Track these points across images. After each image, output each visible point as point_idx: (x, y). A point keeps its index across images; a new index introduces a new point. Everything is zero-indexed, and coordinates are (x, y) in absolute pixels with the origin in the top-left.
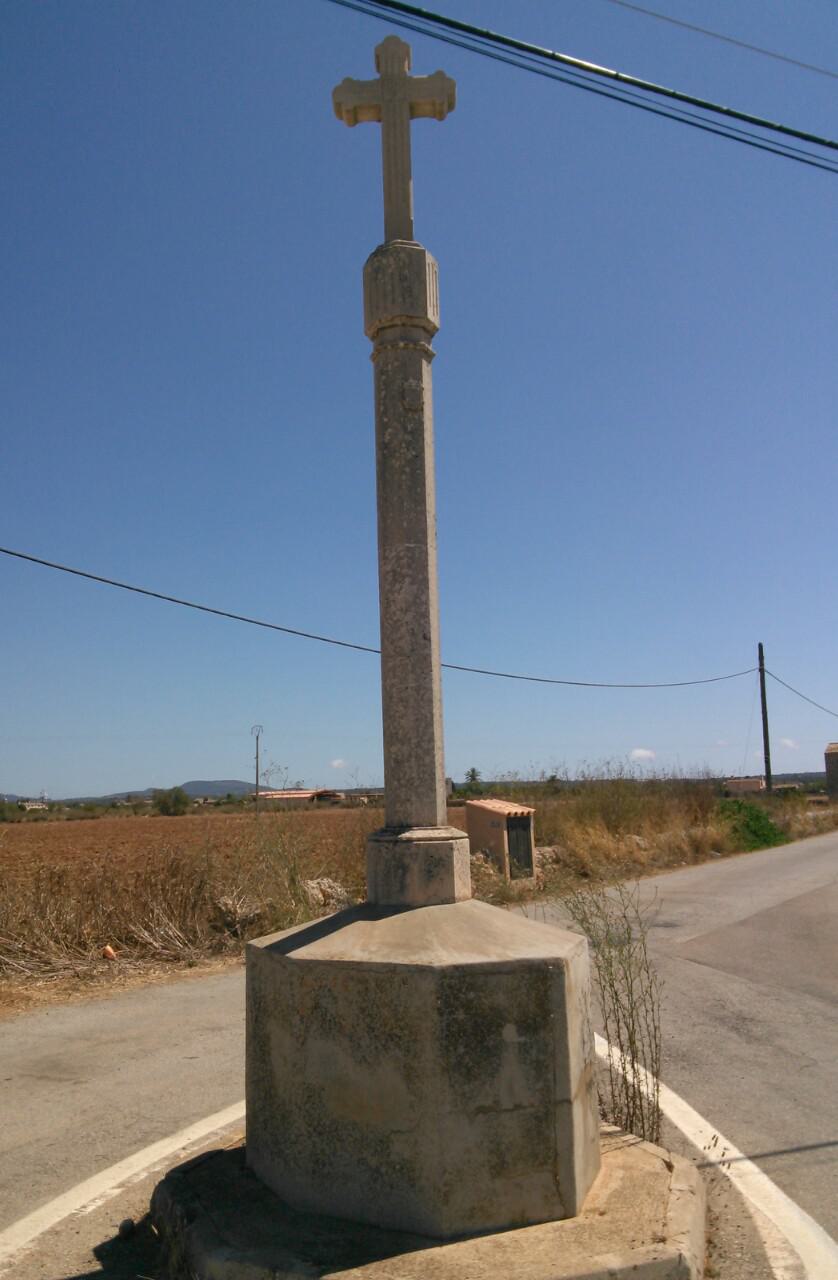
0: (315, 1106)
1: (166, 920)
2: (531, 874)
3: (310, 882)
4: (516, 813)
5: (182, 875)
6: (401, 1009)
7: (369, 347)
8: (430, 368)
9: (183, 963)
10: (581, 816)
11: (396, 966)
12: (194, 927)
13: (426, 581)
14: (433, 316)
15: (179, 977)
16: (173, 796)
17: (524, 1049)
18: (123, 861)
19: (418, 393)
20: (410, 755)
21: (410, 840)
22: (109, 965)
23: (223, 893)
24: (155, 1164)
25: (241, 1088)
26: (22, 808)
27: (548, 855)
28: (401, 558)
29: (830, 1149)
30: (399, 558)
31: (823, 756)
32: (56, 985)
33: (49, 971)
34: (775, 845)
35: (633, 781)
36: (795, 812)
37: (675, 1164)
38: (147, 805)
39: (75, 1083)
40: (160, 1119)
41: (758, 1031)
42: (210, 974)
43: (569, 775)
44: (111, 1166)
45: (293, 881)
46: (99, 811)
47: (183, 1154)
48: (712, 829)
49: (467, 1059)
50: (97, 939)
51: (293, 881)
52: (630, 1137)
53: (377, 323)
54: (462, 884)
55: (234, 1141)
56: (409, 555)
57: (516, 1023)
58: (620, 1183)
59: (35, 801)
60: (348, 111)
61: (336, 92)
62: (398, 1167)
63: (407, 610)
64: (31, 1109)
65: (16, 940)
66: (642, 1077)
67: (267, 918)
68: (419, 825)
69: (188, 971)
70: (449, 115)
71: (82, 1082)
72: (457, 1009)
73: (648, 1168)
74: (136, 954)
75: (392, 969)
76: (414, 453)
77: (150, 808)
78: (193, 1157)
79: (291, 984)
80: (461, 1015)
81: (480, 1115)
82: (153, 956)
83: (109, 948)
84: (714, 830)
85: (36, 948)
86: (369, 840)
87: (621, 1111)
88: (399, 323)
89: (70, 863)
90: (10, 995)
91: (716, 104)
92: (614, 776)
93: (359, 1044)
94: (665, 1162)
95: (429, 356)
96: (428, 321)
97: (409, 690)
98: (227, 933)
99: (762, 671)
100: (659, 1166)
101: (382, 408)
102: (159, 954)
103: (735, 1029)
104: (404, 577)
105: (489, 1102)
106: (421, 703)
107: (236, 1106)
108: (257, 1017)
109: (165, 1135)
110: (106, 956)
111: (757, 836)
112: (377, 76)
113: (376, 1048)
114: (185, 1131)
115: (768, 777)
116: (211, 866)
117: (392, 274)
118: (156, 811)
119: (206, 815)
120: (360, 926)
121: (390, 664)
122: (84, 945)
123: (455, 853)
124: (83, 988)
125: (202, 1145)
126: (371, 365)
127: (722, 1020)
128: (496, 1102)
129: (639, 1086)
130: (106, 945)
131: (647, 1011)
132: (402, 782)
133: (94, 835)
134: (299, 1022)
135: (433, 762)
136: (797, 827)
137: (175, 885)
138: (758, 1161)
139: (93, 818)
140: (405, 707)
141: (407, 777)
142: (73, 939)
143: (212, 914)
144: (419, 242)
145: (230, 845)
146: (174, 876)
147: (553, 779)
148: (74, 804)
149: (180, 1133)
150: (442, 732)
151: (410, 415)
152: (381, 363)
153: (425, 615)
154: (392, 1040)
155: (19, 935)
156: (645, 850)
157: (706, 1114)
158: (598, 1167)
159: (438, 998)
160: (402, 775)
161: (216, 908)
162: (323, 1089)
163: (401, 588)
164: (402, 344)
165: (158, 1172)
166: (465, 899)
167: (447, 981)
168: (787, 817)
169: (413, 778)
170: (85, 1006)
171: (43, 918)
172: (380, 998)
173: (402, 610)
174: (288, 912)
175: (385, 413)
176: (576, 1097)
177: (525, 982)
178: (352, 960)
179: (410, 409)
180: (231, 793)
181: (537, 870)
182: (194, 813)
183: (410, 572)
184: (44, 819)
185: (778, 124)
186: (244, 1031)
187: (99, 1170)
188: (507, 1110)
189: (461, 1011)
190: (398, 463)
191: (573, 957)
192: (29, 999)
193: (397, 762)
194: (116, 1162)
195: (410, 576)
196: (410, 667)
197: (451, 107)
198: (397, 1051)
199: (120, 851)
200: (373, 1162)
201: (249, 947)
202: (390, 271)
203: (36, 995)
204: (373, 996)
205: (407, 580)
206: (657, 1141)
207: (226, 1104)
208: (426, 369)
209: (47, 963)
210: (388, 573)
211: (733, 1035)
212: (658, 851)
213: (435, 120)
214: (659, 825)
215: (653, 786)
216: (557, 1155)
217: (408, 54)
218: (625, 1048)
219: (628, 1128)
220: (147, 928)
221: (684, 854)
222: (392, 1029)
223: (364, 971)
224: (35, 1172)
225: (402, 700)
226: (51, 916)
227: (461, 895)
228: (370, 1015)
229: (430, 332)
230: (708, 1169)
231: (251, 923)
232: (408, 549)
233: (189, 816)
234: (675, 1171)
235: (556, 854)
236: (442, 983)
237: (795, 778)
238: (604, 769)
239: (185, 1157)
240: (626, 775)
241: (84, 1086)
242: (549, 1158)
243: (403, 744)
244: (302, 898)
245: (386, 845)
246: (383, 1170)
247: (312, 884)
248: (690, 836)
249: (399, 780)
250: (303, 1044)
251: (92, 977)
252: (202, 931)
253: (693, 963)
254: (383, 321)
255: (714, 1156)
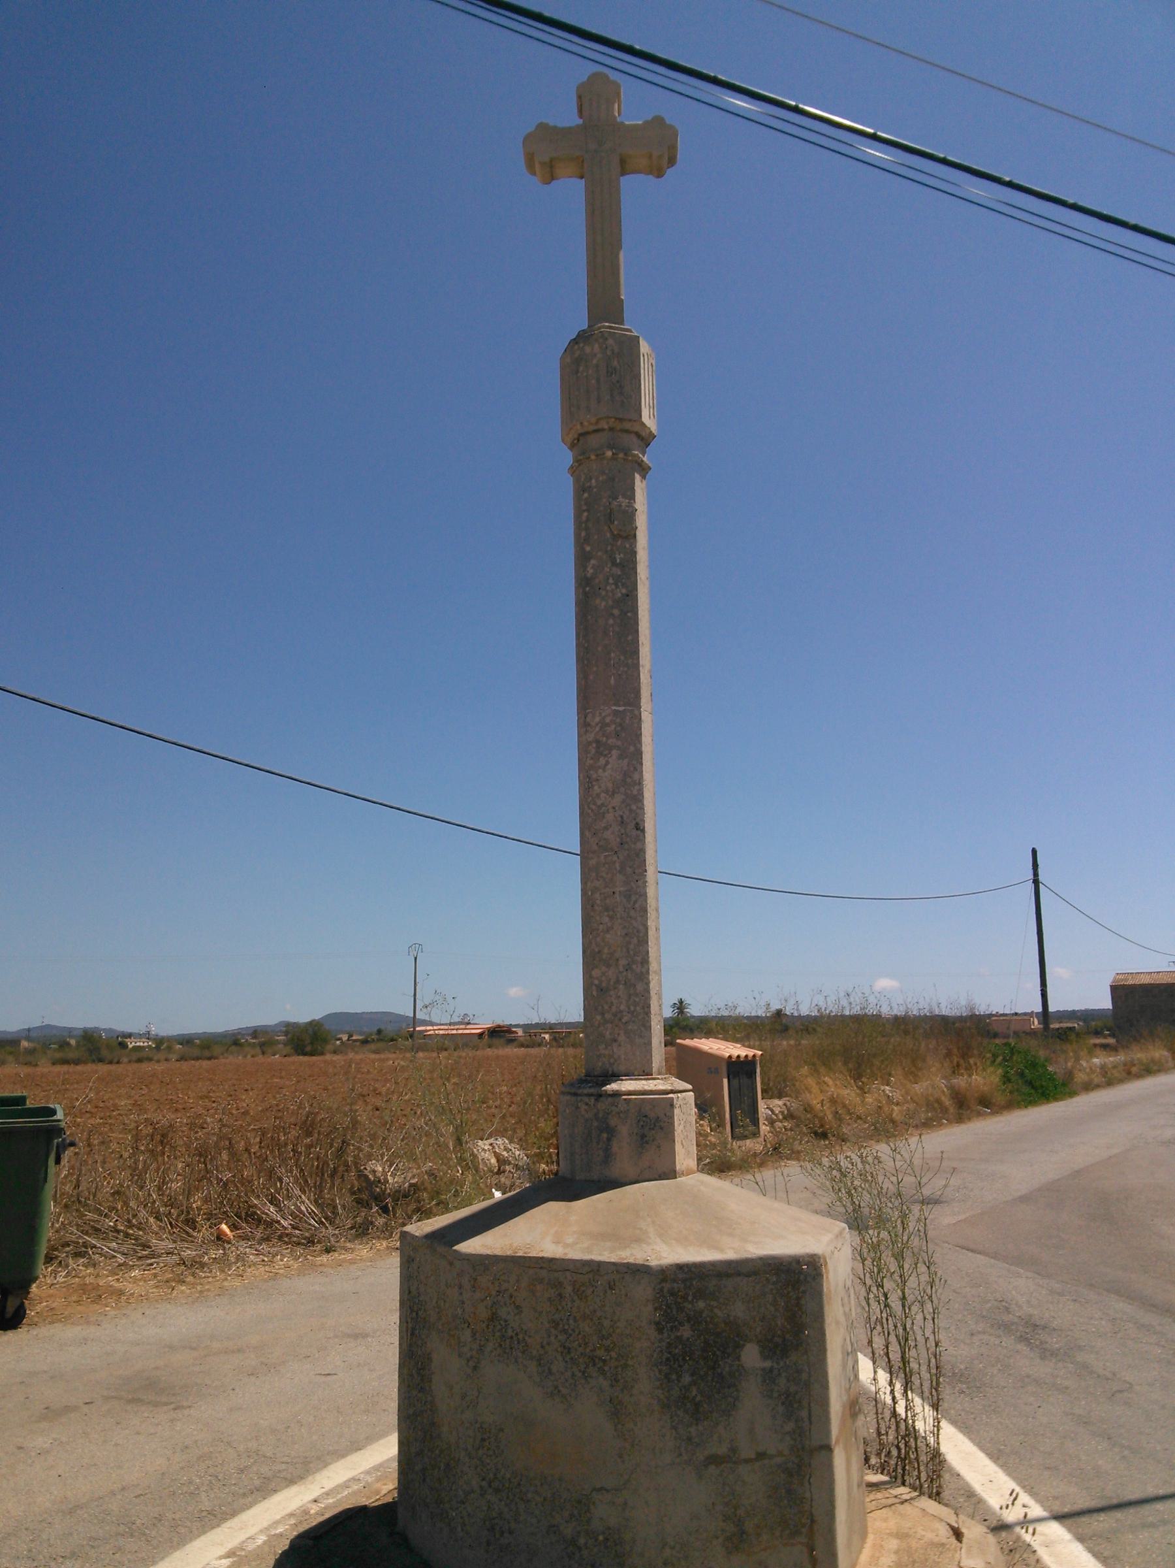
0: (491, 1452)
1: (297, 1192)
2: (756, 1134)
3: (480, 1143)
4: (738, 1057)
5: (319, 1133)
6: (606, 1323)
7: (567, 457)
8: (644, 482)
9: (318, 1247)
10: (822, 1060)
11: (600, 1264)
12: (333, 1200)
13: (639, 754)
14: (648, 418)
15: (313, 1265)
16: (310, 1032)
17: (769, 1376)
18: (246, 1113)
19: (629, 516)
20: (618, 982)
21: (617, 1094)
22: (224, 1249)
23: (369, 1157)
24: (277, 1523)
25: (392, 1417)
26: (123, 1045)
27: (777, 1111)
28: (608, 725)
29: (1159, 1506)
30: (604, 725)
31: (1109, 987)
32: (155, 1275)
33: (147, 1257)
34: (1056, 1099)
35: (879, 1016)
36: (1077, 1059)
37: (964, 1530)
38: (278, 1042)
39: (175, 1409)
40: (285, 1459)
41: (1054, 1342)
42: (352, 1262)
43: (801, 1007)
44: (218, 1526)
45: (459, 1141)
46: (217, 1050)
47: (314, 1509)
48: (979, 1079)
49: (694, 1392)
50: (209, 1216)
51: (459, 1141)
52: (903, 1491)
53: (579, 427)
54: (685, 1154)
55: (384, 1492)
56: (618, 720)
57: (759, 1342)
58: (893, 1557)
59: (140, 1036)
60: (542, 164)
61: (528, 139)
62: (601, 1538)
63: (613, 793)
64: (116, 1445)
65: (106, 1216)
66: (918, 1409)
67: (425, 1189)
68: (629, 1075)
69: (324, 1258)
70: (670, 172)
71: (183, 1407)
72: (681, 1324)
73: (929, 1536)
74: (259, 1236)
75: (595, 1268)
76: (624, 591)
77: (281, 1046)
78: (327, 1515)
79: (460, 1287)
80: (686, 1332)
81: (712, 1468)
82: (280, 1238)
83: (224, 1227)
84: (984, 1079)
85: (131, 1226)
86: (563, 1093)
87: (889, 1454)
88: (606, 427)
89: (179, 1115)
90: (97, 1287)
91: (997, 175)
92: (856, 1010)
93: (549, 1369)
94: (952, 1528)
95: (644, 470)
96: (643, 424)
97: (617, 895)
98: (375, 1209)
99: (1036, 882)
100: (944, 1533)
101: (583, 534)
102: (287, 1235)
103: (1023, 1339)
104: (610, 749)
105: (723, 1450)
106: (632, 913)
107: (389, 1438)
108: (413, 1329)
109: (291, 1482)
110: (220, 1238)
111: (1033, 1087)
112: (580, 122)
113: (573, 1375)
114: (318, 1476)
115: (1045, 1014)
116: (355, 1123)
117: (597, 366)
118: (288, 1049)
119: (351, 1055)
120: (553, 1208)
121: (593, 862)
122: (191, 1223)
123: (677, 1111)
124: (190, 1279)
125: (339, 1496)
126: (569, 481)
127: (1006, 1327)
128: (733, 1450)
129: (914, 1422)
130: (221, 1223)
131: (925, 1319)
132: (608, 1016)
133: (210, 1080)
134: (470, 1339)
135: (648, 991)
136: (1080, 1077)
137: (310, 1146)
138: (1069, 1522)
139: (209, 1059)
140: (611, 918)
141: (614, 1009)
142: (178, 1216)
143: (356, 1183)
144: (631, 325)
145: (380, 1094)
146: (309, 1134)
147: (779, 1013)
148: (187, 1041)
149: (310, 1478)
150: (659, 950)
151: (619, 543)
152: (583, 477)
153: (637, 798)
154: (594, 1365)
155: (112, 1209)
156: (898, 1104)
157: (996, 1456)
158: (864, 1536)
159: (656, 1309)
160: (606, 1007)
161: (361, 1176)
162: (502, 1430)
163: (607, 763)
164: (609, 453)
165: (281, 1535)
166: (689, 1172)
167: (667, 1286)
168: (1069, 1064)
169: (621, 1012)
170: (193, 1303)
171: (141, 1188)
172: (579, 1308)
173: (607, 792)
174: (452, 1181)
175: (587, 540)
176: (837, 1441)
177: (771, 1286)
178: (541, 1255)
179: (620, 536)
180: (383, 1027)
181: (764, 1128)
182: (335, 1052)
183: (619, 743)
184: (150, 1059)
185: (1071, 201)
186: (396, 1340)
187: (203, 1531)
188: (747, 1461)
189: (687, 1326)
190: (603, 604)
191: (833, 1253)
192: (121, 1293)
193: (601, 990)
194: (225, 1520)
195: (618, 748)
196: (617, 865)
197: (672, 161)
198: (601, 1379)
199: (244, 1101)
200: (568, 1531)
201: (404, 1235)
202: (595, 362)
203: (129, 1287)
204: (570, 1305)
205: (615, 753)
206: (936, 1496)
207: (371, 1439)
208: (640, 487)
209: (145, 1246)
210: (590, 743)
211: (1021, 1347)
212: (912, 1106)
213: (651, 177)
214: (913, 1074)
215: (904, 1025)
216: (813, 1521)
217: (618, 94)
218: (894, 1369)
219: (898, 1478)
220: (273, 1201)
221: (945, 1110)
222: (594, 1350)
223: (556, 1271)
224: (118, 1534)
225: (607, 909)
226: (151, 1186)
227: (684, 1168)
228: (565, 1331)
229: (646, 439)
230: (1004, 1534)
231: (405, 1196)
232: (616, 713)
233: (328, 1057)
234: (965, 1540)
235: (788, 1110)
236: (662, 1290)
237: (1072, 1015)
238: (844, 1003)
239: (319, 1513)
240: (871, 1010)
241: (186, 1412)
242: (804, 1526)
243: (609, 966)
244: (471, 1164)
245: (586, 1099)
246: (582, 1541)
247: (484, 1144)
248: (951, 1088)
249: (603, 1014)
250: (475, 1368)
251: (202, 1265)
252: (344, 1207)
253: (964, 1251)
254: (586, 424)
255: (1011, 1516)
